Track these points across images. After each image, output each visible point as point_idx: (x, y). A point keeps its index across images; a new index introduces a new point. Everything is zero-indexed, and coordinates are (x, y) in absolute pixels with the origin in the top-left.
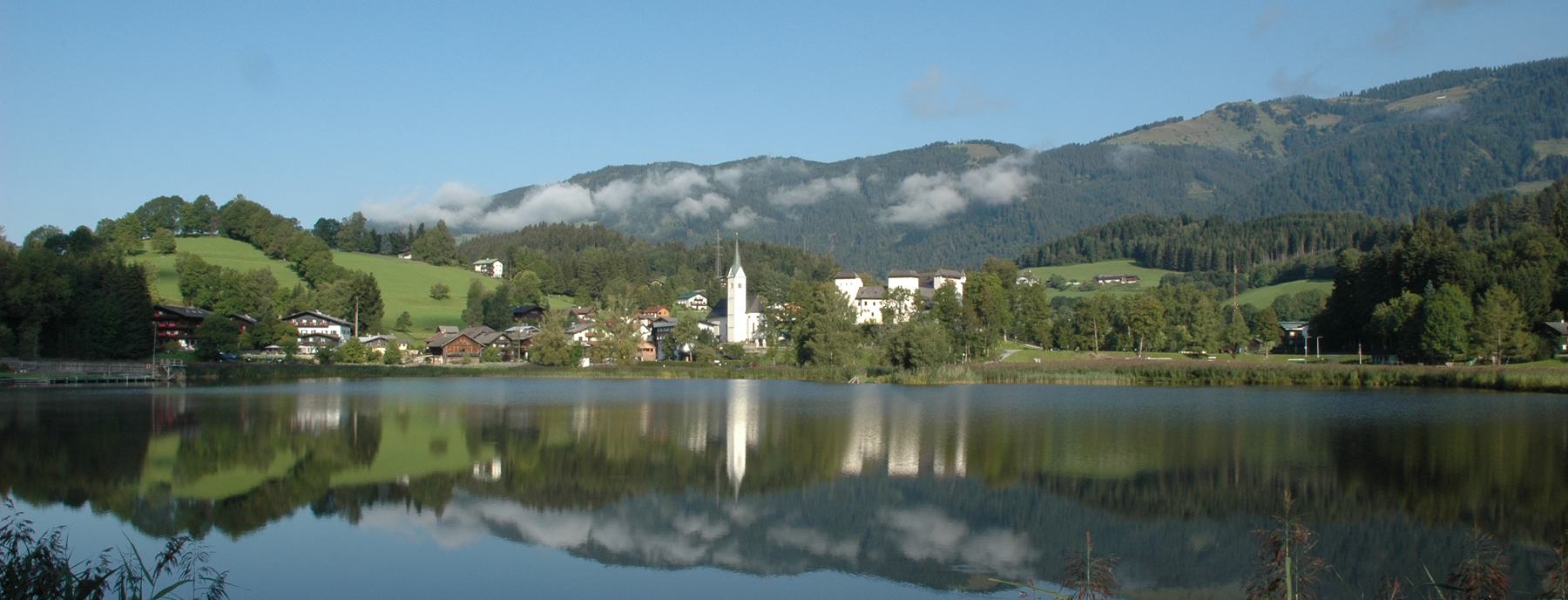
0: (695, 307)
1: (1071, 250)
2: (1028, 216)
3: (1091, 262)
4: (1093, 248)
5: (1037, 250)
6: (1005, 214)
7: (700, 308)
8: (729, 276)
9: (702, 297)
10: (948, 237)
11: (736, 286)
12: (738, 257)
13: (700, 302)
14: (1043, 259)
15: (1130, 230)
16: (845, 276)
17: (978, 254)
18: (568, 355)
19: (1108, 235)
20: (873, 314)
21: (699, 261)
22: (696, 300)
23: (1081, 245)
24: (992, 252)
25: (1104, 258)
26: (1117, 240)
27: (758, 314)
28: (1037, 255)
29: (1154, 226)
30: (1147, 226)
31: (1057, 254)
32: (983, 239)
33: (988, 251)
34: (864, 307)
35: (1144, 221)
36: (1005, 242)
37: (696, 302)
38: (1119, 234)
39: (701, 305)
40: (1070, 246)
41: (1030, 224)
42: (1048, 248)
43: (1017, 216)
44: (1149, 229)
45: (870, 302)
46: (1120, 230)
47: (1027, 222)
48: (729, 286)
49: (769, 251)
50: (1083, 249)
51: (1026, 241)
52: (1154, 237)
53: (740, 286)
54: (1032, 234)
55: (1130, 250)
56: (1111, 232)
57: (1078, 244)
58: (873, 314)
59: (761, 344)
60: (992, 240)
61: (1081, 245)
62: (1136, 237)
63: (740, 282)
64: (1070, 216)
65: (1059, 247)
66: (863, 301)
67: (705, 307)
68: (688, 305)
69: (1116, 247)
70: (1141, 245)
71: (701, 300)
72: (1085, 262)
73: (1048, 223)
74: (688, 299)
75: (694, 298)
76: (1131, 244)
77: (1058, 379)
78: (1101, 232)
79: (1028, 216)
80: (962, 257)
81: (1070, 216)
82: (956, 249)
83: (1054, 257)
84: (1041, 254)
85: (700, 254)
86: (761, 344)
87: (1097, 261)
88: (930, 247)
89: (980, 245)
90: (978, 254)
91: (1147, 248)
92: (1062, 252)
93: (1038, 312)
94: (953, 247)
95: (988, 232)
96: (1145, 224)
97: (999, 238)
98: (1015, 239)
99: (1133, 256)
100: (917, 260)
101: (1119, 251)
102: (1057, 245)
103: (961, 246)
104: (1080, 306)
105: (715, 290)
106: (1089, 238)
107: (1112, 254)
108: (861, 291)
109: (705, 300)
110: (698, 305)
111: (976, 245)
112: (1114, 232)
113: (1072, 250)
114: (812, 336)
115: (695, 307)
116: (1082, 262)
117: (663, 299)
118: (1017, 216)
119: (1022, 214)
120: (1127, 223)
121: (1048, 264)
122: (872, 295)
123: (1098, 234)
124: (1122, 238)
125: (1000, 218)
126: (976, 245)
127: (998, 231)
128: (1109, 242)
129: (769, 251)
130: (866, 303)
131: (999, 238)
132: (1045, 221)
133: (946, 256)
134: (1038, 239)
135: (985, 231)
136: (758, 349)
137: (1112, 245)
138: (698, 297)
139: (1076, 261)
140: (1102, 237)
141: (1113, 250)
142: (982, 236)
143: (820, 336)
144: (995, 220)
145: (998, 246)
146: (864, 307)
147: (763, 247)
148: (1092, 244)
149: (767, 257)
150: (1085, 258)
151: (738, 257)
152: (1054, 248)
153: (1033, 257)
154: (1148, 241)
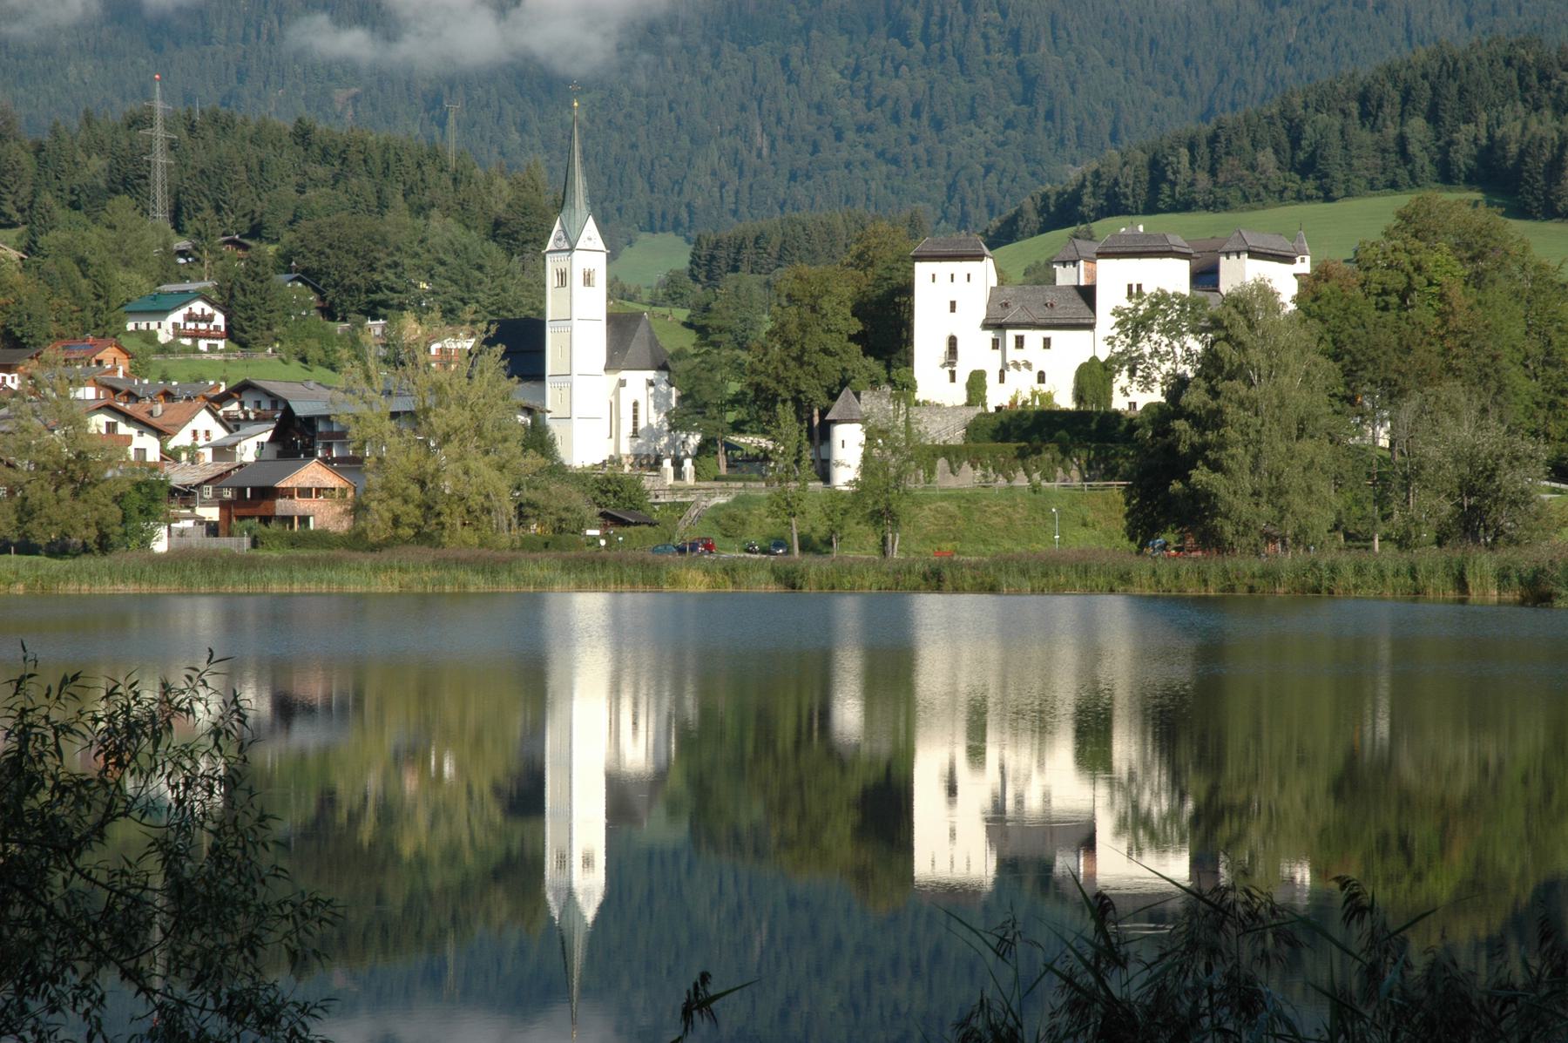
0: (187, 342)
1: (1261, 157)
2: (1015, 41)
3: (1328, 198)
4: (1335, 151)
5: (1141, 158)
6: (935, 30)
7: (203, 344)
8: (550, 245)
9: (208, 310)
10: (743, 108)
11: (577, 279)
12: (580, 183)
13: (202, 326)
14: (1166, 188)
15: (1462, 91)
16: (951, 250)
17: (848, 165)
18: (117, 512)
19: (1387, 110)
20: (1041, 377)
21: (77, 180)
22: (190, 317)
23: (1295, 142)
24: (895, 161)
25: (1372, 185)
26: (1417, 126)
27: (651, 374)
28: (1145, 177)
29: (1544, 77)
30: (1521, 80)
31: (1213, 172)
32: (863, 116)
33: (881, 155)
34: (1013, 354)
35: (1508, 62)
36: (938, 125)
37: (191, 325)
38: (1425, 105)
39: (207, 335)
40: (1255, 144)
41: (1021, 68)
42: (1184, 151)
43: (976, 38)
44: (1524, 87)
45: (1033, 337)
46: (1429, 93)
47: (1009, 59)
48: (551, 279)
49: (325, 153)
50: (1301, 156)
51: (1009, 125)
52: (1548, 113)
53: (588, 280)
54: (1026, 101)
55: (1463, 156)
56: (1398, 99)
57: (1284, 140)
58: (1041, 377)
59: (679, 475)
60: (896, 118)
61: (1295, 142)
62: (1483, 117)
63: (589, 266)
64: (1153, 43)
65: (1221, 148)
66: (1011, 335)
67: (221, 344)
68: (164, 336)
69: (1414, 148)
70: (1504, 142)
71: (210, 319)
72: (1309, 198)
73: (1080, 62)
74: (164, 312)
75: (185, 310)
76: (1466, 139)
77: (233, 704)
78: (1363, 99)
79: (1015, 41)
80: (793, 177)
81: (1153, 43)
82: (772, 147)
83: (1203, 179)
84: (1157, 170)
85: (80, 157)
86: (679, 475)
87: (1349, 194)
88: (685, 141)
89: (850, 135)
90: (848, 165)
91: (1522, 153)
92: (1231, 167)
93: (1550, 371)
94: (762, 141)
95: (878, 93)
96: (1514, 75)
97: (916, 113)
98: (973, 115)
99: (1471, 180)
100: (640, 184)
101: (1422, 159)
102: (1213, 140)
103: (790, 140)
104: (103, 337)
105: (251, 284)
106: (1323, 118)
107: (1402, 173)
108: (998, 301)
109: (220, 320)
110: (196, 335)
111: (839, 137)
112: (1407, 97)
113: (1267, 158)
114: (1211, 455)
115: (187, 342)
116: (1300, 197)
117: (89, 314)
118: (976, 38)
119: (993, 33)
120: (1450, 68)
121: (1186, 206)
122: (1042, 315)
123: (1354, 107)
124: (1433, 117)
125: (920, 46)
126: (839, 137)
127: (912, 92)
128: (1392, 131)
129: (325, 153)
130: (1047, 343)
131: (916, 113)
132: (1071, 56)
133: (741, 174)
134: (1050, 116)
135: (868, 89)
136: (673, 490)
137: (1402, 141)
138: (198, 307)
139: (1281, 196)
140: (1364, 115)
141: (1404, 155)
142: (859, 104)
143: (1238, 456)
144: (902, 51)
145: (914, 140)
146: (1013, 354)
147: (303, 135)
148: (1334, 138)
149: (321, 172)
150: (1310, 186)
151: (580, 183)
152: (1203, 149)
153: (1132, 180)
154: (1525, 127)
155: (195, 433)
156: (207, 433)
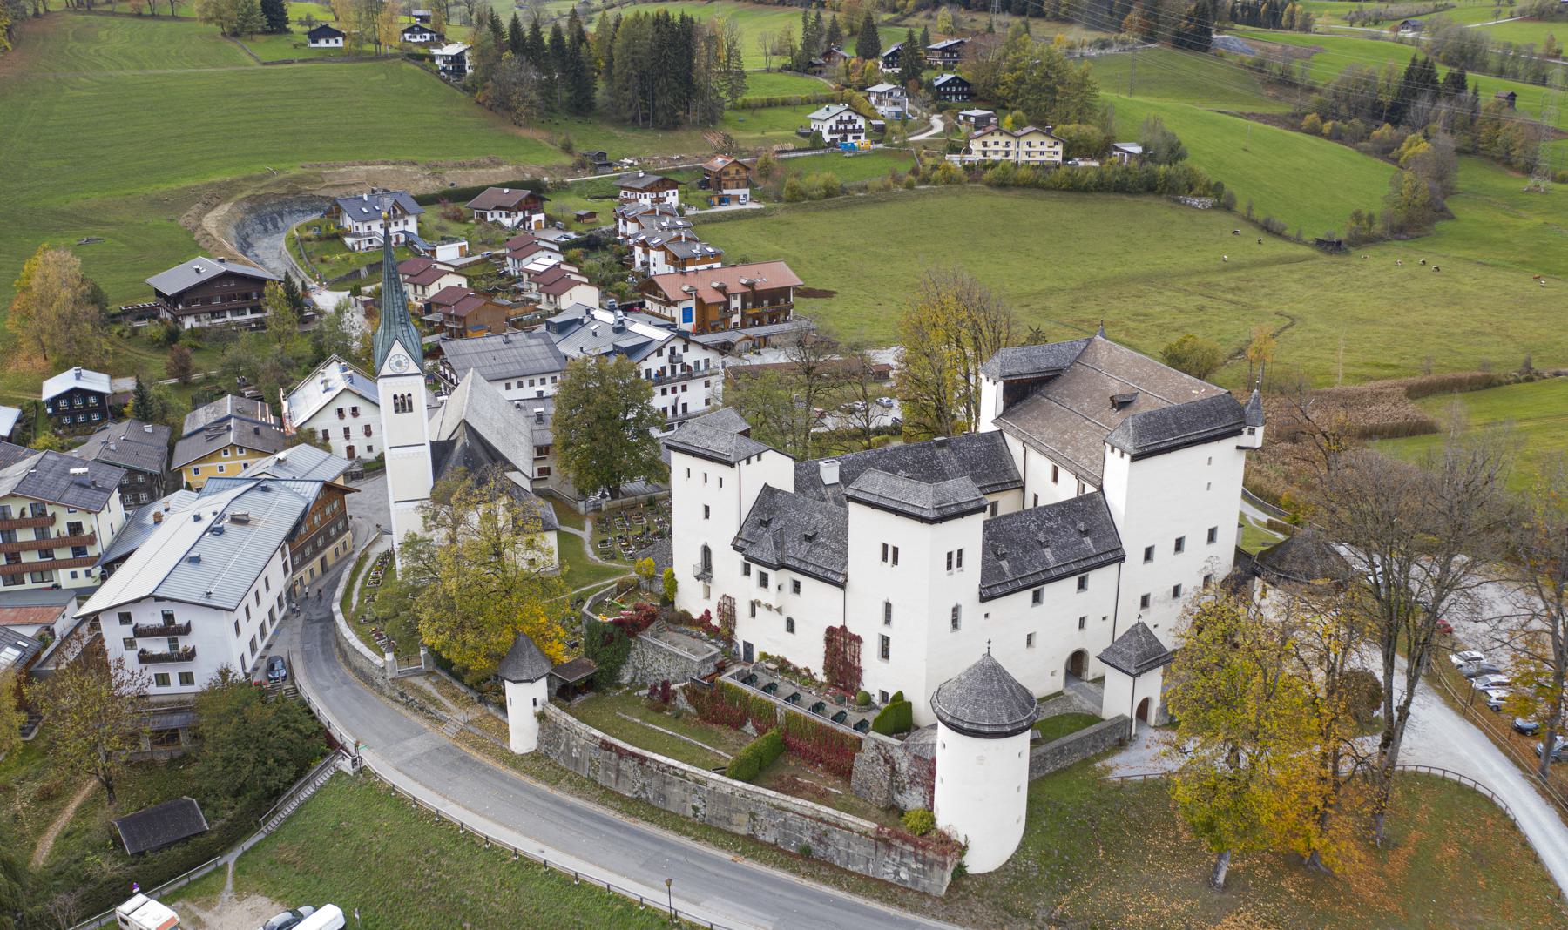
13: (850, 127)
20: (791, 626)
22: (841, 121)
37: (841, 126)
110: (846, 131)
155: (340, 412)
156: (354, 409)
